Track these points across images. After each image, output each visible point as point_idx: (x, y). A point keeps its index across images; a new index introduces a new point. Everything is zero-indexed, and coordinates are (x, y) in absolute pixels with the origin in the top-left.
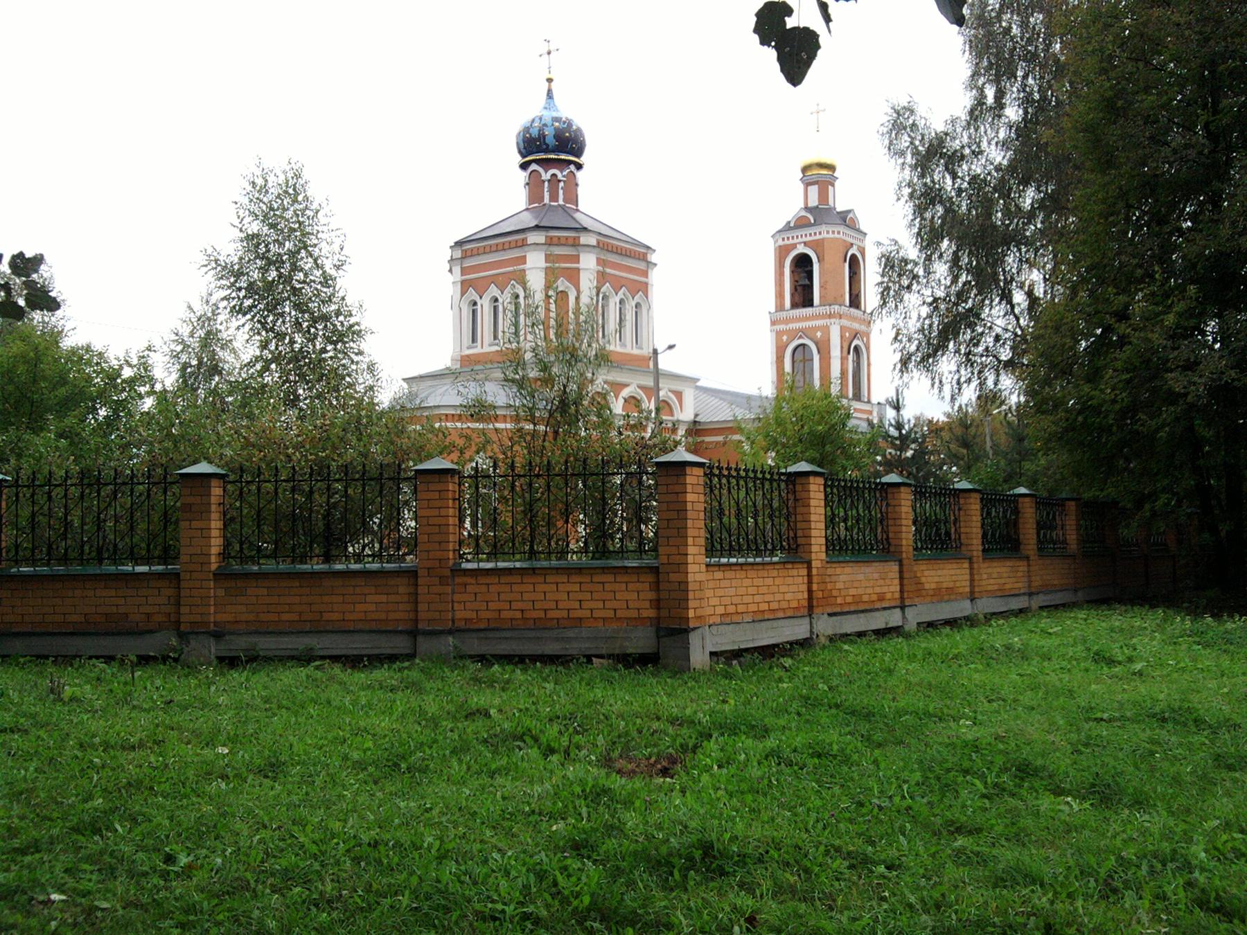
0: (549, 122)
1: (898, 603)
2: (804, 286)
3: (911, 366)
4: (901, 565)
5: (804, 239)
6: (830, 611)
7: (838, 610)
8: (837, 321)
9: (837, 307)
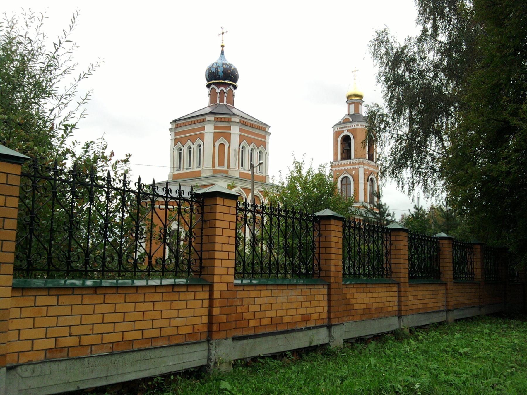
0: (221, 65)
1: (326, 322)
2: (347, 150)
3: (387, 174)
4: (329, 289)
5: (347, 128)
6: (238, 334)
7: (251, 332)
8: (362, 166)
9: (362, 160)
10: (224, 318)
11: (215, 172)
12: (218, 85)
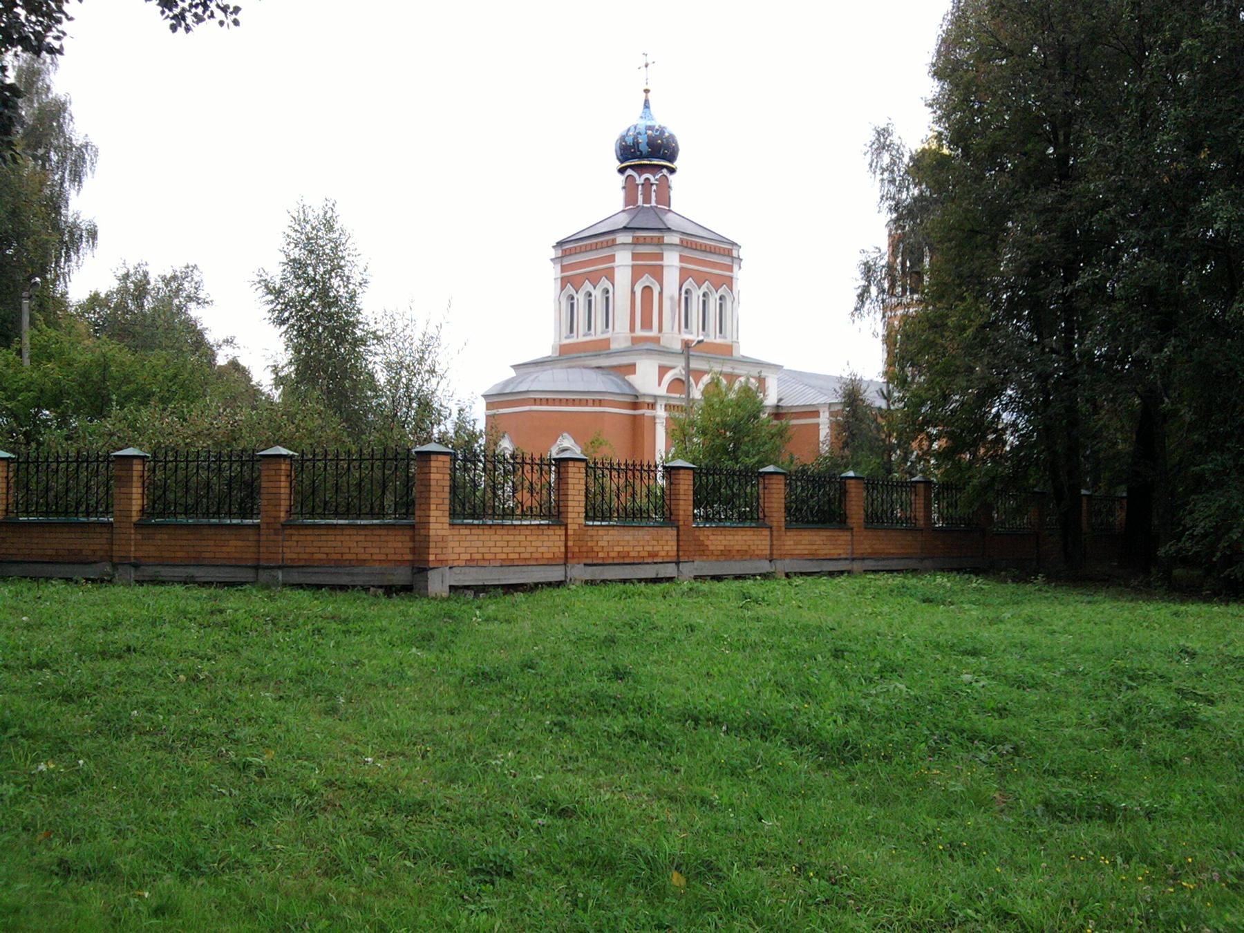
0: (643, 131)
6: (589, 561)
7: (600, 562)
10: (577, 550)
11: (635, 340)
12: (640, 168)
